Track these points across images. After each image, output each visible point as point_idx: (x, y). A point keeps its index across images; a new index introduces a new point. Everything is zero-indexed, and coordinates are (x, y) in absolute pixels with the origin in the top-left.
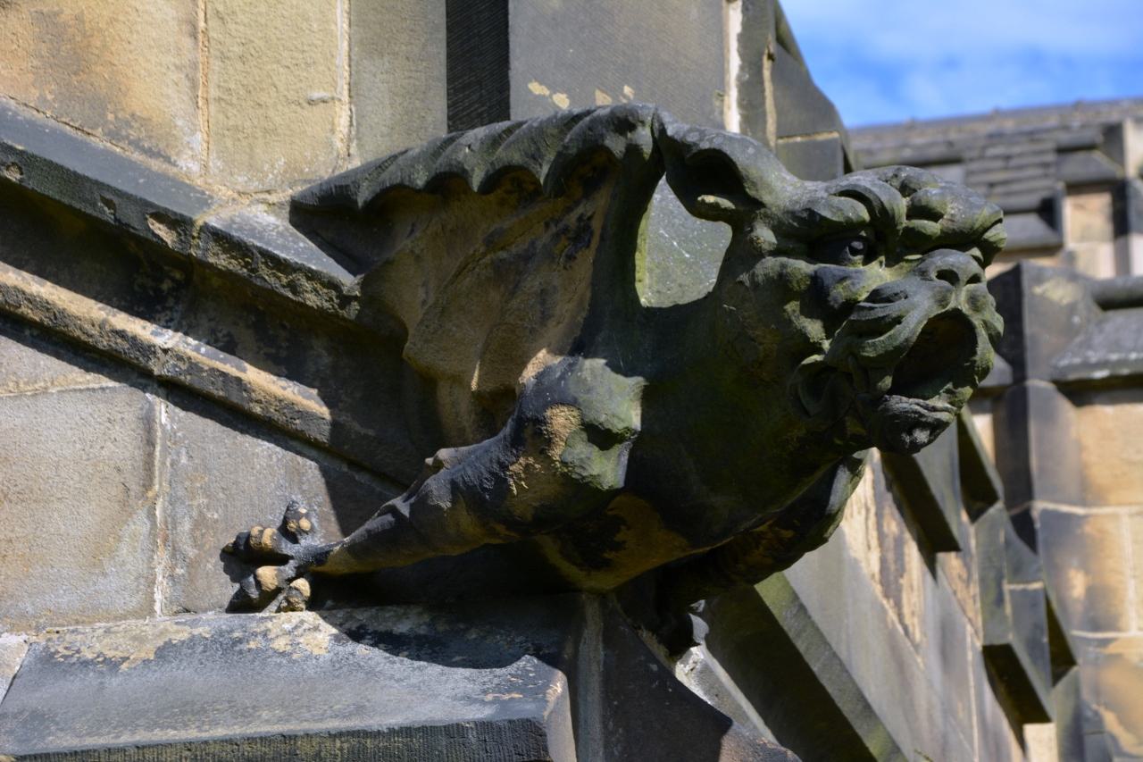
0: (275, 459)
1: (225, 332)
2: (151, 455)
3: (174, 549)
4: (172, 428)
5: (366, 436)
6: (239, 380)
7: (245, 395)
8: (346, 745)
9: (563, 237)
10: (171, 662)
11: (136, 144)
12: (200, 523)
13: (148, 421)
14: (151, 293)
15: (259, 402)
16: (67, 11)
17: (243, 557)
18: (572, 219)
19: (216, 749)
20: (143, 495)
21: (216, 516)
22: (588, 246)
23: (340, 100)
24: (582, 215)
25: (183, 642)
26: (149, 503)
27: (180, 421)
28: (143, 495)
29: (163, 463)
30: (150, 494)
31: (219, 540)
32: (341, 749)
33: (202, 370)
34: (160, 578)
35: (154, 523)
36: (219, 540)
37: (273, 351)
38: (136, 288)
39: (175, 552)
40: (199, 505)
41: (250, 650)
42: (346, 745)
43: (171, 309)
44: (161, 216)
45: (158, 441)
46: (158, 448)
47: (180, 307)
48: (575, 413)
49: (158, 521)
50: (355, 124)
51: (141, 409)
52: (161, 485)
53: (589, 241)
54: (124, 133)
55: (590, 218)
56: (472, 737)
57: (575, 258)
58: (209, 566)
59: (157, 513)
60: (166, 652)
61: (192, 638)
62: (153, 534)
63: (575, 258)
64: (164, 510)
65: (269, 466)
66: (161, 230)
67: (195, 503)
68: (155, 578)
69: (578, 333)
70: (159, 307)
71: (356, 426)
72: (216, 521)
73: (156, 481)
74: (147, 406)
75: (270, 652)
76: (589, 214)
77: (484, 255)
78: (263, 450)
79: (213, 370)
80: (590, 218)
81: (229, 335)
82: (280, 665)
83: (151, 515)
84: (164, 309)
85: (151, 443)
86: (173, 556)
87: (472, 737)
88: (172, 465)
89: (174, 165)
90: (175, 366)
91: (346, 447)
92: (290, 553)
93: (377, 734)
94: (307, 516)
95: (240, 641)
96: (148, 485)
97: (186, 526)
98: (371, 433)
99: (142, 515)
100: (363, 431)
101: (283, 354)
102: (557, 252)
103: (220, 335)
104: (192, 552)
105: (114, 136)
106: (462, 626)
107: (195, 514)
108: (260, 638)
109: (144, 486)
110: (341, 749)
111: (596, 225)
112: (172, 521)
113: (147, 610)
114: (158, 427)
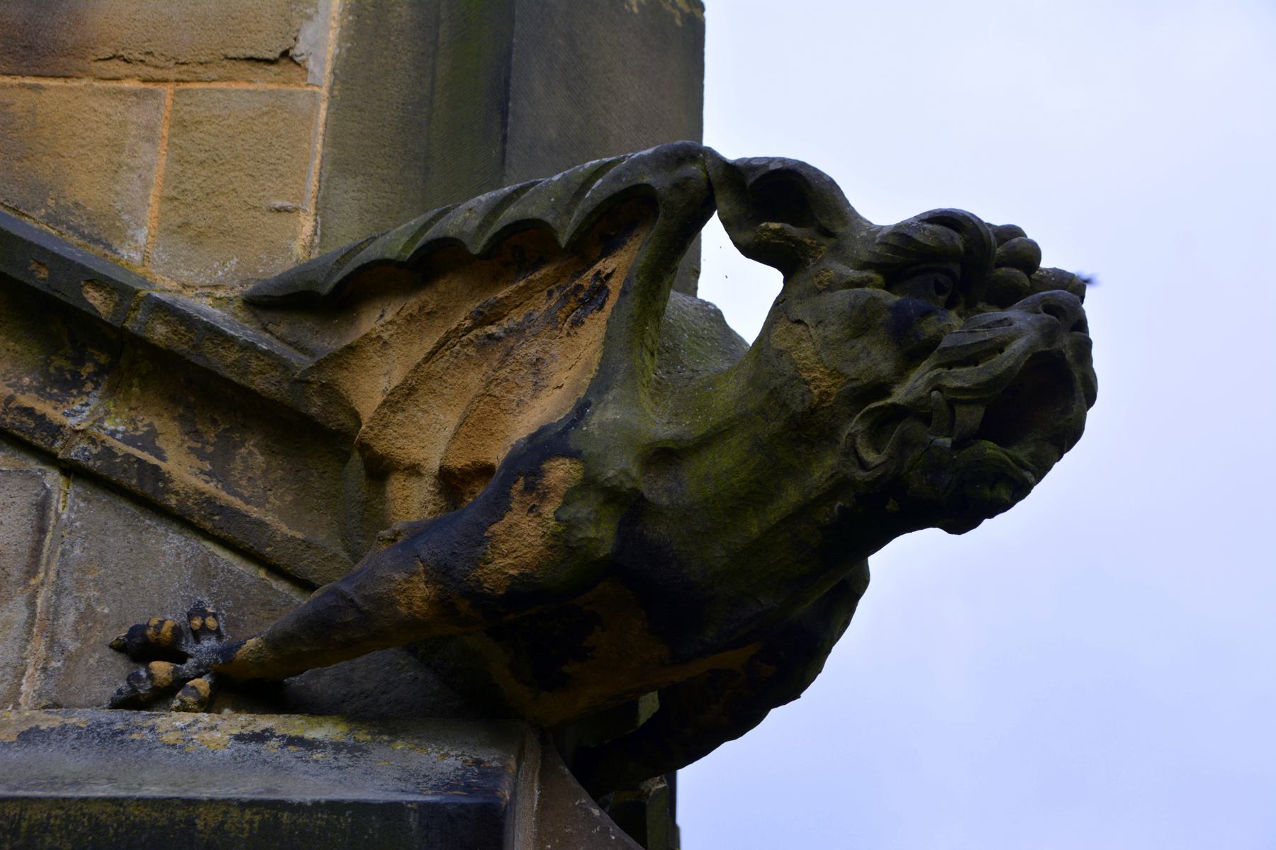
0: (183, 559)
1: (147, 421)
2: (40, 542)
3: (52, 640)
4: (69, 517)
5: (293, 538)
6: (157, 468)
7: (161, 485)
8: (257, 818)
9: (572, 299)
10: (36, 745)
11: (75, 229)
12: (87, 615)
13: (42, 507)
14: (68, 376)
15: (177, 493)
16: (19, 104)
17: (139, 647)
18: (587, 278)
19: (95, 809)
20: (26, 583)
21: (106, 611)
22: (601, 308)
23: (305, 211)
24: (599, 272)
25: (53, 729)
26: (29, 591)
27: (78, 511)
28: (26, 583)
29: (52, 552)
30: (33, 582)
31: (106, 636)
32: (251, 822)
33: (116, 456)
34: (30, 670)
35: (33, 614)
36: (106, 636)
37: (199, 445)
38: (52, 370)
39: (53, 642)
40: (89, 598)
41: (133, 741)
42: (257, 818)
43: (88, 394)
44: (100, 282)
45: (51, 528)
46: (49, 536)
47: (98, 393)
48: (579, 466)
49: (39, 610)
50: (319, 232)
51: (37, 495)
52: (46, 574)
53: (604, 302)
54: (63, 218)
55: (609, 276)
56: (413, 821)
57: (583, 323)
58: (91, 661)
59: (39, 602)
60: (29, 736)
61: (64, 726)
62: (30, 624)
63: (583, 323)
64: (48, 600)
65: (175, 565)
66: (95, 298)
67: (85, 595)
68: (26, 669)
69: (582, 394)
70: (75, 392)
71: (284, 529)
72: (107, 616)
73: (42, 569)
74: (43, 493)
75: (158, 744)
76: (609, 271)
77: (469, 330)
78: (171, 545)
79: (128, 456)
80: (609, 276)
81: (150, 425)
82: (170, 755)
83: (31, 604)
84: (81, 393)
85: (42, 530)
86: (50, 648)
87: (413, 821)
88: (62, 555)
89: (115, 252)
90: (85, 449)
91: (268, 549)
92: (190, 651)
93: (299, 808)
94: (214, 615)
95: (122, 732)
96: (32, 571)
97: (71, 617)
98: (299, 535)
99: (20, 600)
100: (290, 533)
101: (210, 449)
102: (563, 316)
103: (140, 424)
104: (73, 646)
105: (53, 219)
106: (386, 738)
107: (82, 607)
108: (146, 731)
109: (27, 572)
110: (251, 822)
111: (615, 285)
112: (55, 613)
113: (13, 697)
114: (52, 514)
